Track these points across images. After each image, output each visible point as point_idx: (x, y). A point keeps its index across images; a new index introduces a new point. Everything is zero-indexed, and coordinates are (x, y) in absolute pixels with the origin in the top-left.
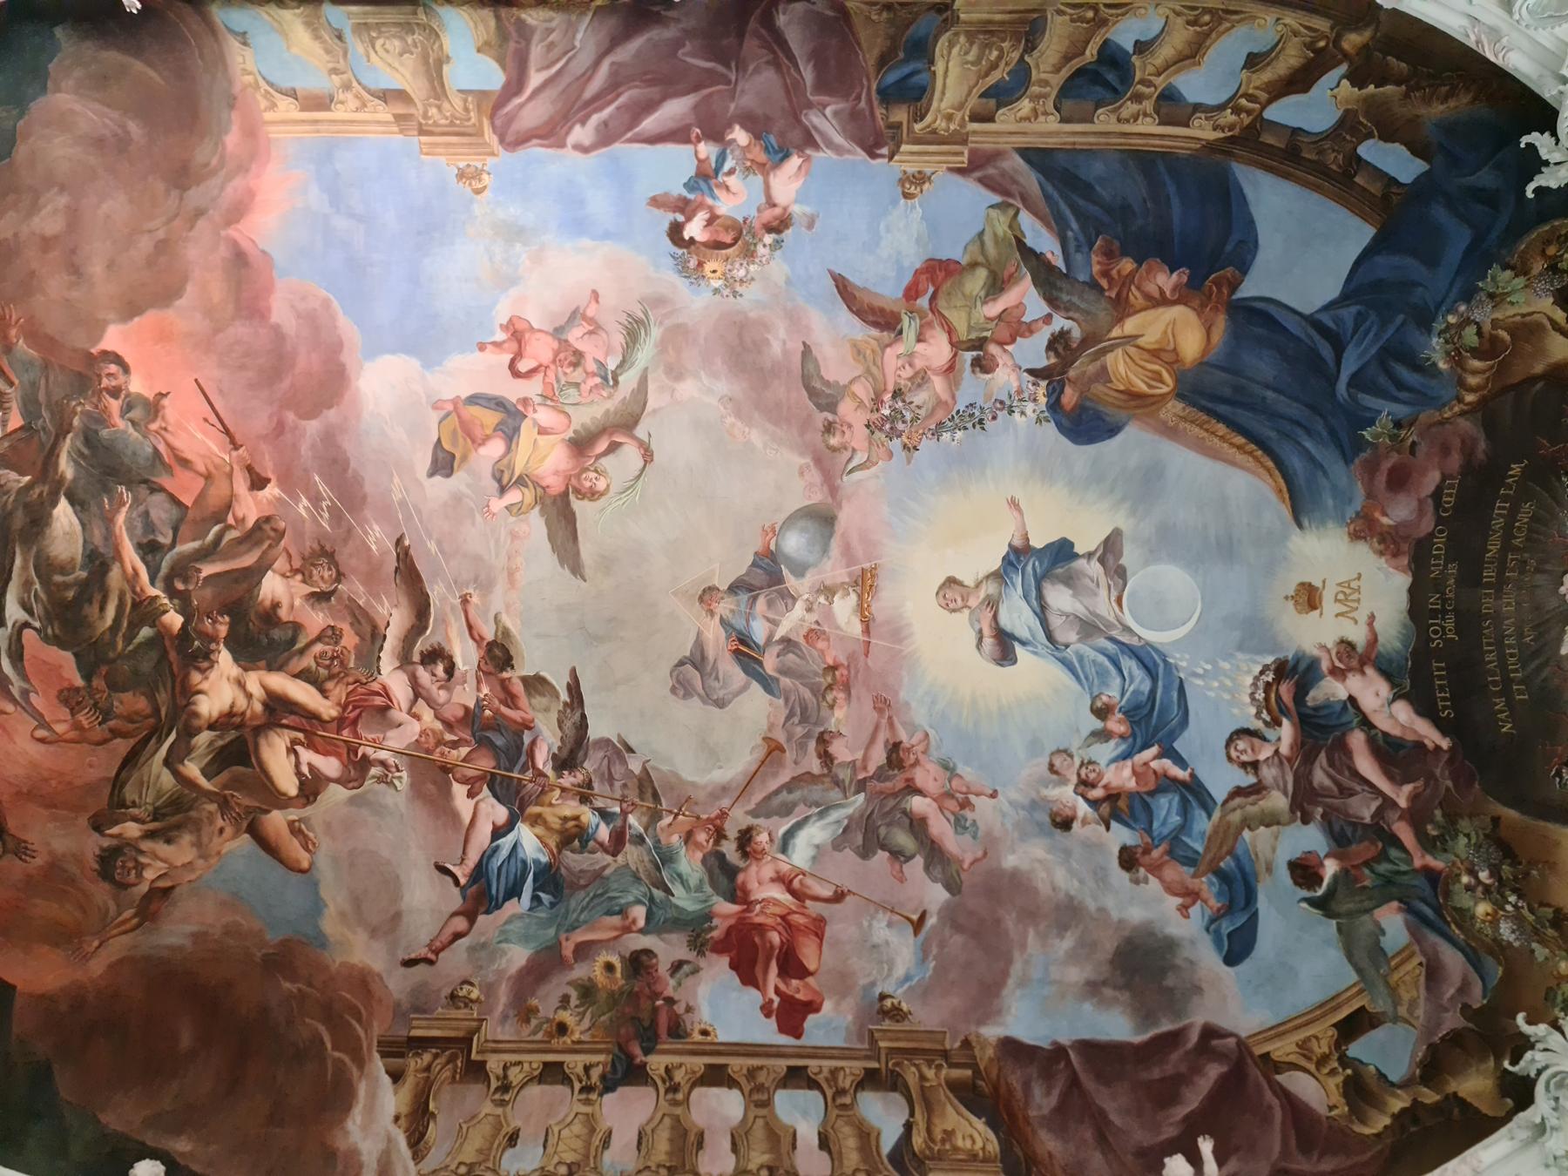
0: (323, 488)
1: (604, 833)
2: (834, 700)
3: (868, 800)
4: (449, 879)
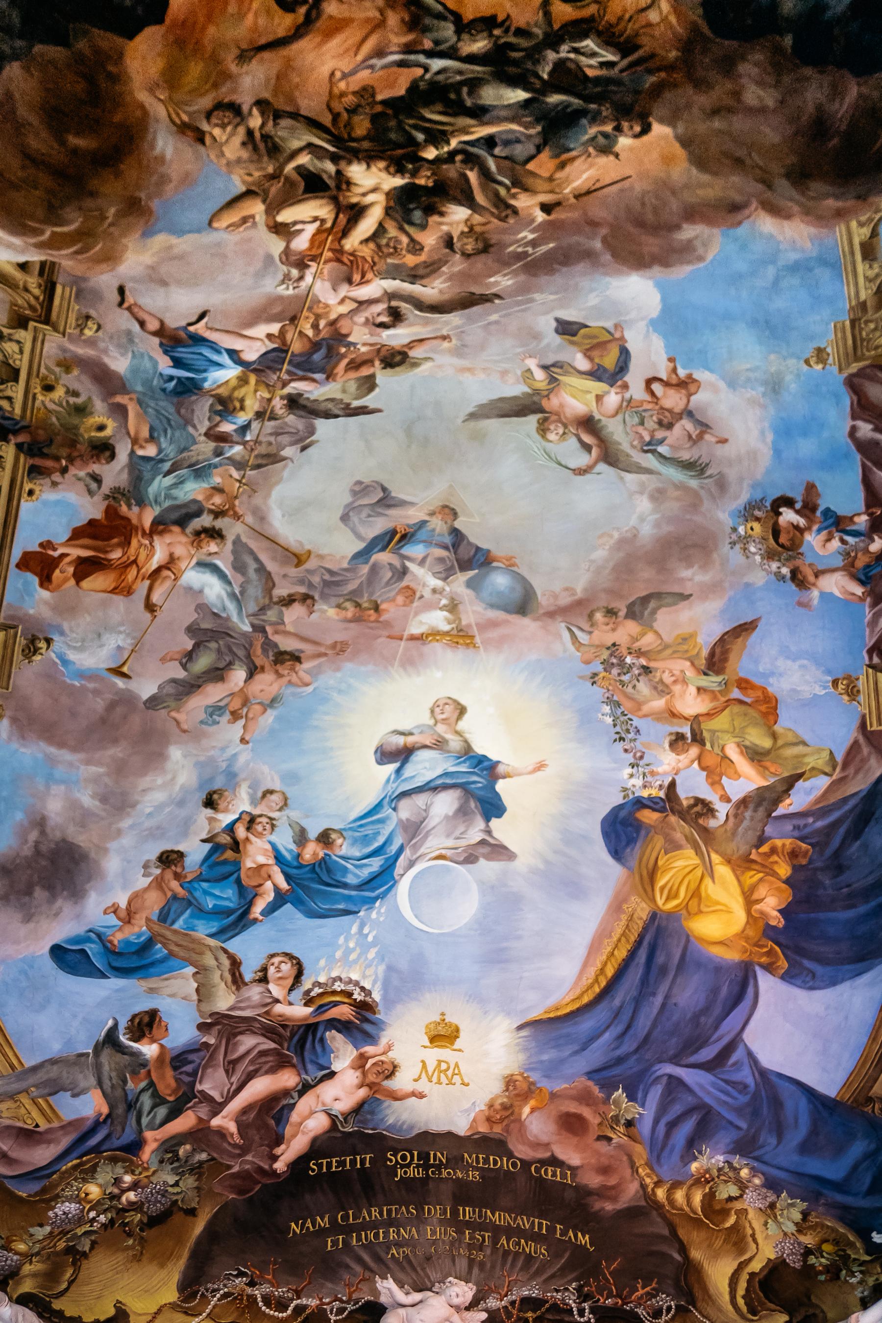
0: (544, 249)
1: (227, 427)
2: (345, 609)
3: (244, 634)
4: (194, 319)
